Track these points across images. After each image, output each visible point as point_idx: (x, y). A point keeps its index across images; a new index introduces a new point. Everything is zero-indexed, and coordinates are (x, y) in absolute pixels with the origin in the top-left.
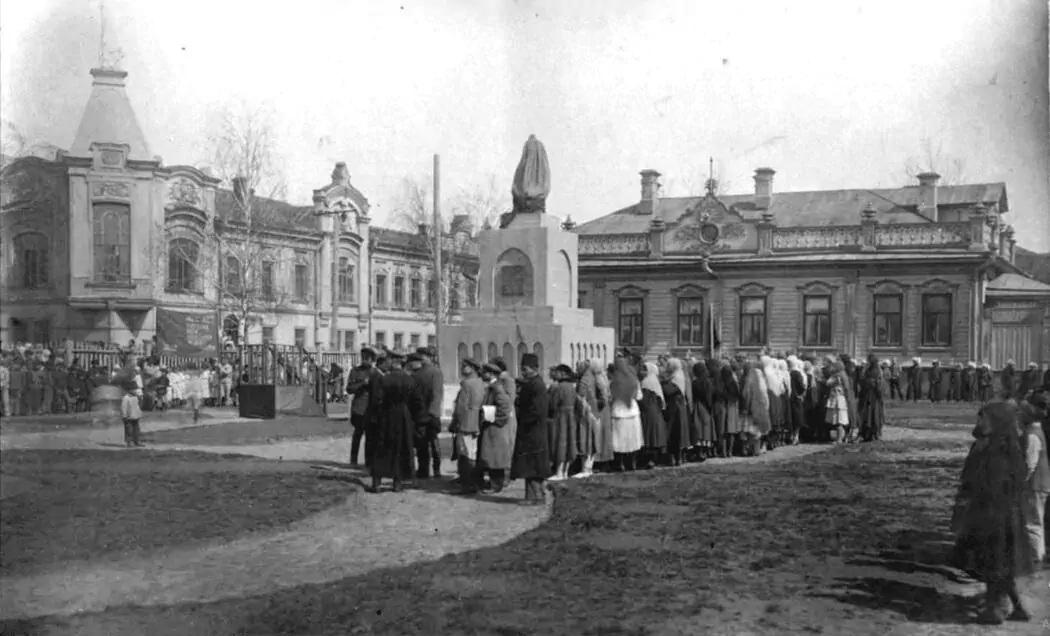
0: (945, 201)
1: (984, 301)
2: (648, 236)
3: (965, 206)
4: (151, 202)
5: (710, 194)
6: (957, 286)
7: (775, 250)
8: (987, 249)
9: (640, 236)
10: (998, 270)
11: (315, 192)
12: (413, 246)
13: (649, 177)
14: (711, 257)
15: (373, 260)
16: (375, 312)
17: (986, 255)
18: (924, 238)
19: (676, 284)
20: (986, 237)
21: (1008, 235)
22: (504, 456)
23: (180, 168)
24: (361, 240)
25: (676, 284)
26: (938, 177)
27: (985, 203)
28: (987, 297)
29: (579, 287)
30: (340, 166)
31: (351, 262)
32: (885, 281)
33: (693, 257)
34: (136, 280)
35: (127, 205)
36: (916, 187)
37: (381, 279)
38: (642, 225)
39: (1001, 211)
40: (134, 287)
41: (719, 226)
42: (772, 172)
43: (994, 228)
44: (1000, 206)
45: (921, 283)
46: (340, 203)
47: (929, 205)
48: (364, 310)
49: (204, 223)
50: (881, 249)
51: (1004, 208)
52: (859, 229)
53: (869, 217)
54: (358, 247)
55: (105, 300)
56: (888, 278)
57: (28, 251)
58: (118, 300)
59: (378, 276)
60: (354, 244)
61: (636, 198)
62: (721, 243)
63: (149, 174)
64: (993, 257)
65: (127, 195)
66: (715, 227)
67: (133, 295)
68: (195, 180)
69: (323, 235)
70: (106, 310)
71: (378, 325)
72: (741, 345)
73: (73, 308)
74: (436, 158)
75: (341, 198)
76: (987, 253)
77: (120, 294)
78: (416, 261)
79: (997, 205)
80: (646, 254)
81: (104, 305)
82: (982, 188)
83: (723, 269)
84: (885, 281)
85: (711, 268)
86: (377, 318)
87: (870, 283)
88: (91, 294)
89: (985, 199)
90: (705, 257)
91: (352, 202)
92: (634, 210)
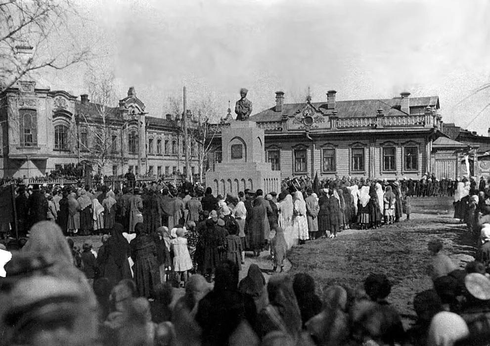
0: (412, 105)
1: (431, 150)
2: (280, 122)
3: (422, 107)
4: (44, 108)
5: (309, 103)
6: (420, 144)
7: (338, 128)
8: (432, 127)
9: (278, 122)
10: (438, 135)
11: (120, 101)
12: (171, 125)
13: (280, 94)
14: (310, 131)
15: (147, 132)
16: (149, 157)
17: (432, 129)
18: (404, 121)
19: (294, 144)
20: (432, 121)
21: (439, 119)
22: (306, 236)
23: (58, 92)
24: (71, 115)
25: (294, 144)
26: (409, 94)
27: (431, 106)
28: (433, 148)
29: (265, 145)
30: (131, 89)
31: (136, 133)
32: (387, 142)
33: (301, 132)
34: (40, 145)
35: (35, 110)
36: (399, 98)
37: (151, 141)
38: (278, 116)
39: (437, 109)
40: (39, 149)
41: (313, 117)
42: (335, 92)
43: (434, 117)
44: (437, 107)
45: (404, 142)
46: (131, 106)
47: (406, 106)
48: (144, 156)
49: (70, 118)
50: (386, 127)
51: (438, 107)
52: (375, 118)
53: (380, 113)
54: (70, 118)
55: (26, 155)
56: (391, 140)
57: (279, 170)
58: (31, 155)
59: (150, 139)
60: (68, 117)
61: (273, 104)
62: (314, 125)
63: (45, 95)
64: (435, 131)
65: (35, 105)
66: (311, 118)
67: (39, 152)
68: (66, 97)
69: (124, 121)
70: (23, 161)
71: (150, 163)
72: (241, 157)
73: (11, 159)
74: (184, 88)
75: (132, 104)
76: (433, 129)
77: (34, 152)
78: (159, 131)
79: (435, 106)
80: (280, 129)
81: (26, 157)
82: (429, 98)
83: (316, 137)
84: (387, 142)
85: (310, 136)
86: (149, 159)
87: (381, 143)
88: (19, 152)
89: (430, 104)
90: (307, 131)
91: (137, 105)
92: (274, 109)
